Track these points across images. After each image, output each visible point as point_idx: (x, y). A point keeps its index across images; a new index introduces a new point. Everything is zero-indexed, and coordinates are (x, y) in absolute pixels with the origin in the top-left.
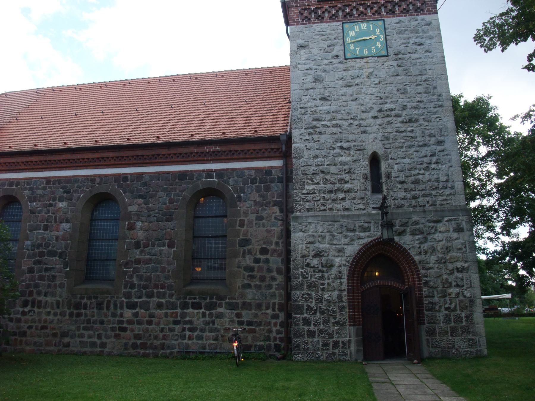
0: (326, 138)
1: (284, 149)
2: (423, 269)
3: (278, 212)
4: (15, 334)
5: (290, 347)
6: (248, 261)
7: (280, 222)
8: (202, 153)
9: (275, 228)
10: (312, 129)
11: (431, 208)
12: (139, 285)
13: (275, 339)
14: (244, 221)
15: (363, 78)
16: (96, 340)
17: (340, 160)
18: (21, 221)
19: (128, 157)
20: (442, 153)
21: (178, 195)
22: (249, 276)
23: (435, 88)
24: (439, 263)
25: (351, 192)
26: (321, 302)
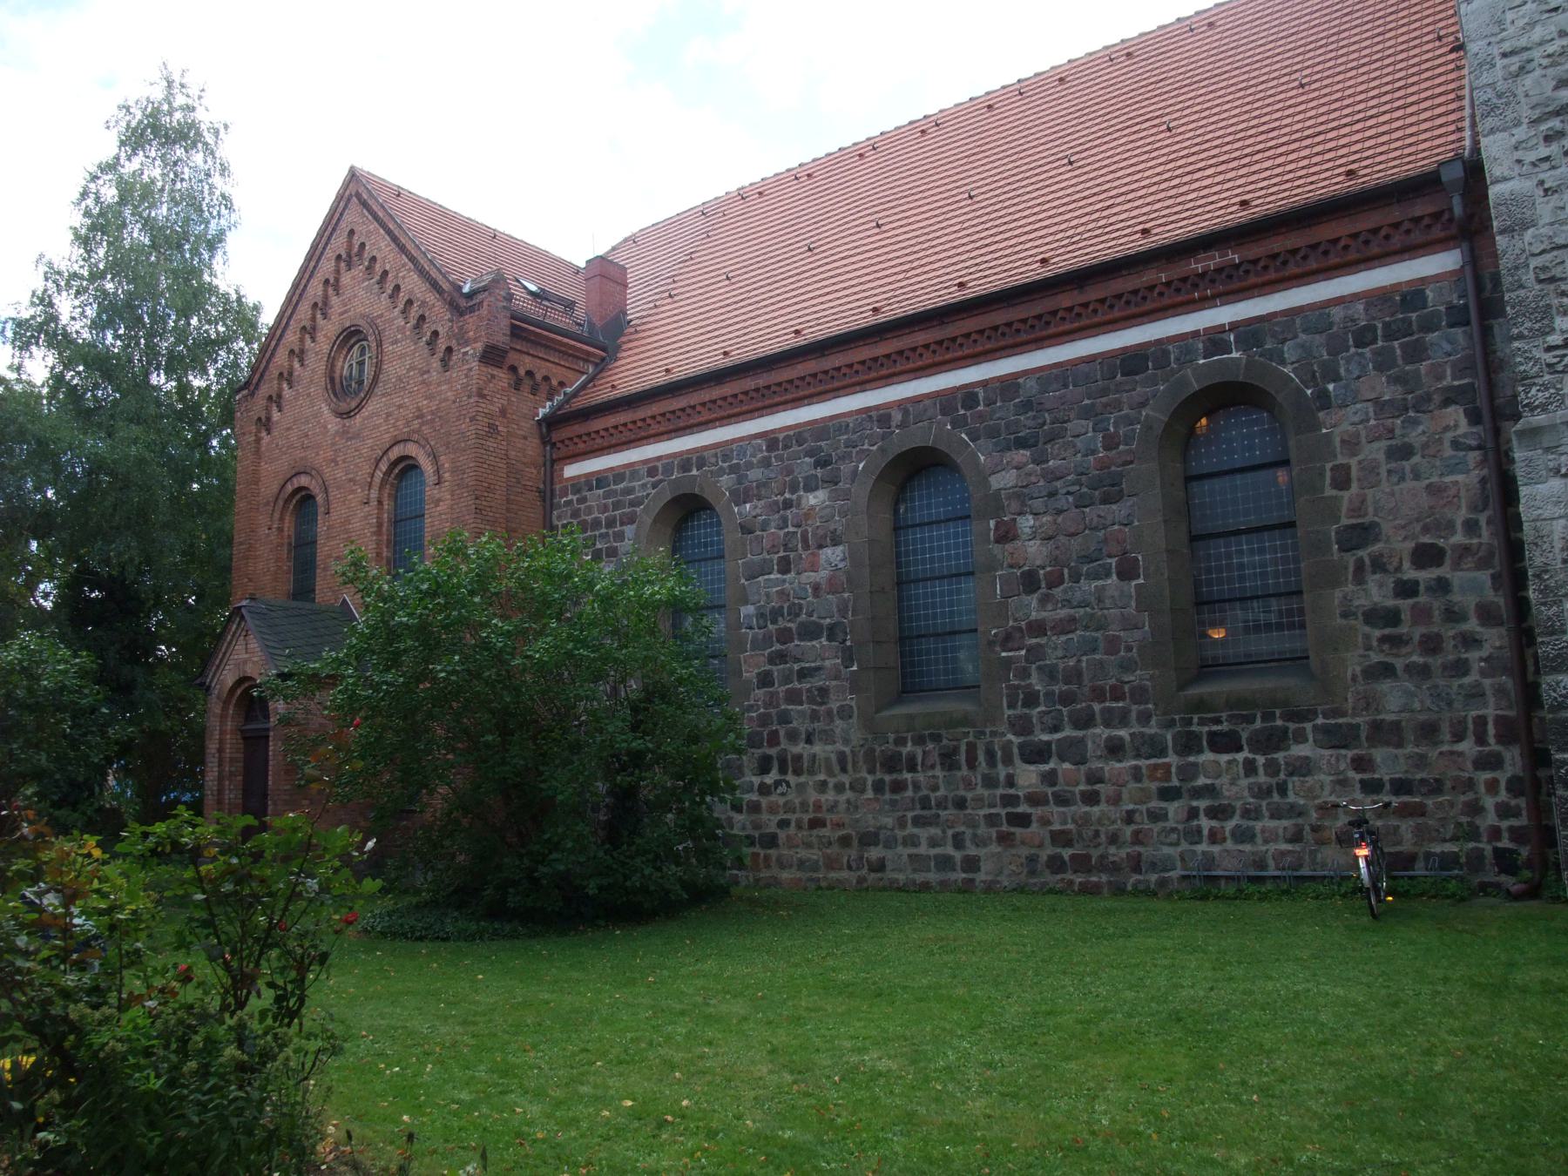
1: (1458, 210)
3: (1463, 421)
4: (751, 841)
6: (1377, 592)
7: (1474, 456)
8: (1184, 280)
9: (1460, 478)
12: (1049, 694)
13: (1495, 833)
14: (1347, 468)
16: (949, 850)
18: (722, 557)
22: (1383, 639)
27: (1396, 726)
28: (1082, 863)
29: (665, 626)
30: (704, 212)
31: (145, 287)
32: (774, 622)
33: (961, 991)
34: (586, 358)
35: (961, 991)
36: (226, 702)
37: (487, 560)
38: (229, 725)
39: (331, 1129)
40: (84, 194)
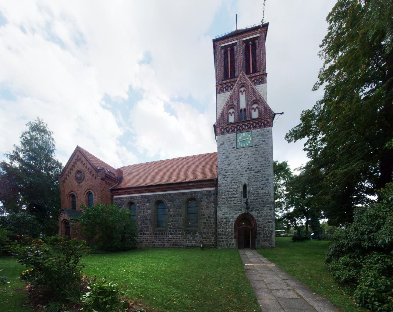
1: (215, 184)
2: (258, 222)
4: (139, 242)
6: (204, 220)
11: (262, 202)
13: (213, 242)
23: (268, 159)
27: (205, 233)
28: (175, 245)
31: (38, 155)
33: (163, 258)
34: (117, 182)
36: (62, 222)
39: (84, 276)
40: (22, 136)
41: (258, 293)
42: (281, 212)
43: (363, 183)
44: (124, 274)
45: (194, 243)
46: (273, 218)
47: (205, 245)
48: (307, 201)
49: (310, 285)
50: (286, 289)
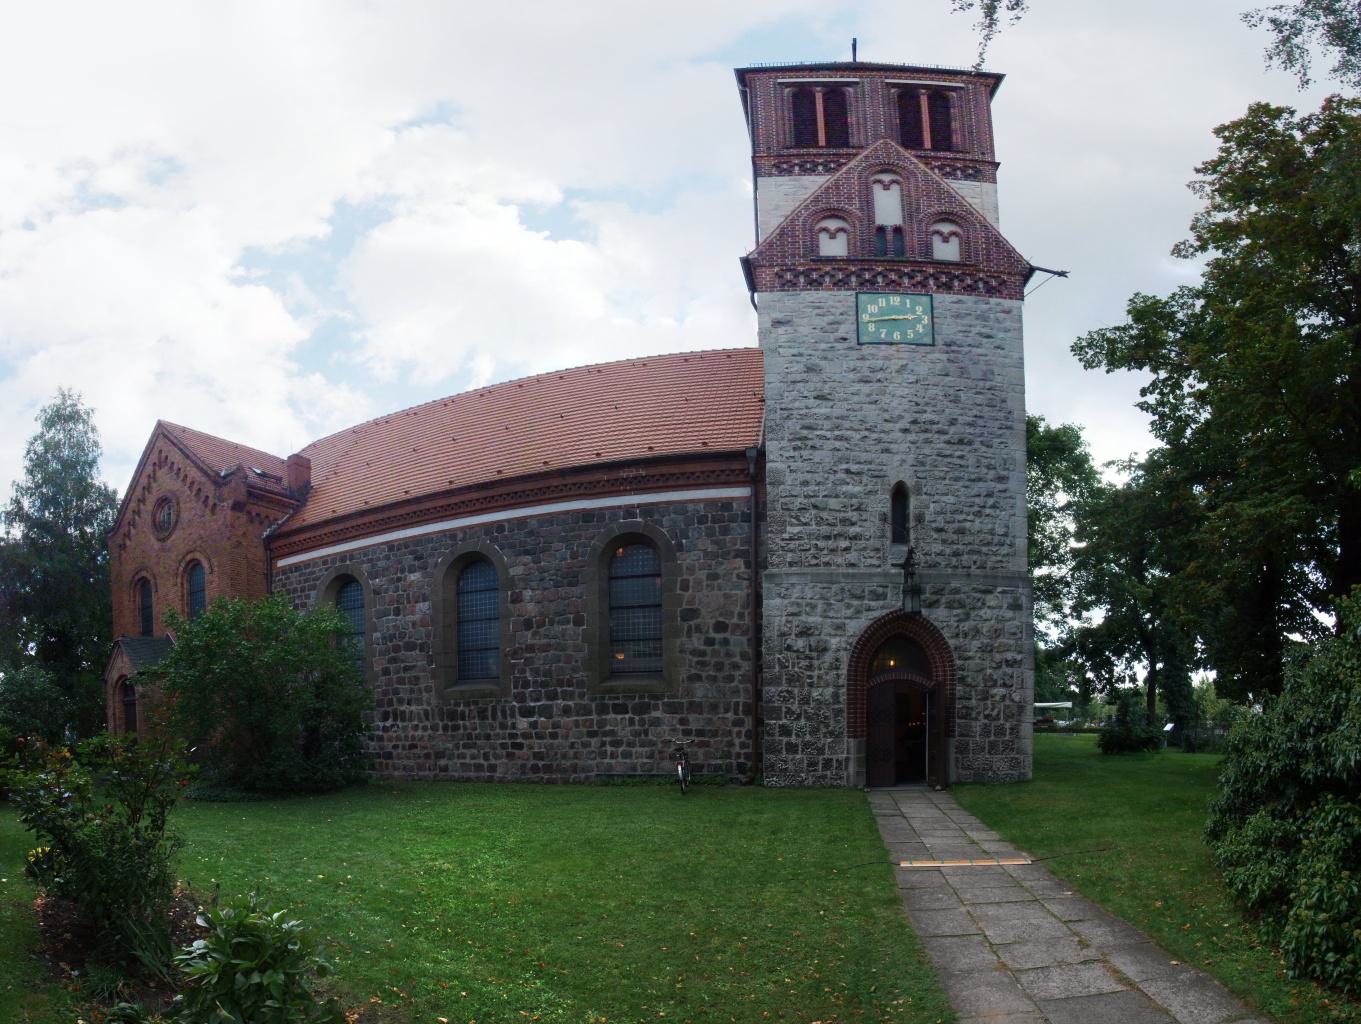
0: (823, 456)
1: (752, 470)
2: (960, 658)
3: (743, 566)
4: (378, 756)
5: (760, 767)
6: (697, 642)
7: (746, 583)
8: (616, 480)
9: (739, 592)
10: (800, 442)
11: (978, 572)
12: (535, 682)
13: (738, 755)
14: (688, 580)
15: (891, 373)
16: (482, 761)
17: (844, 489)
18: (363, 607)
19: (501, 496)
20: (1003, 495)
21: (585, 546)
22: (698, 663)
23: (1004, 401)
24: (983, 651)
25: (860, 539)
26: (808, 703)
28: (548, 769)
29: (333, 643)
30: (354, 431)
31: (60, 488)
32: (391, 641)
33: (485, 831)
34: (289, 506)
35: (485, 831)
37: (238, 611)
38: (117, 699)
41: (962, 991)
42: (1056, 623)
43: (1306, 569)
44: (317, 889)
45: (640, 758)
46: (1026, 648)
47: (697, 768)
48: (1151, 590)
49: (1160, 930)
50: (1077, 959)
